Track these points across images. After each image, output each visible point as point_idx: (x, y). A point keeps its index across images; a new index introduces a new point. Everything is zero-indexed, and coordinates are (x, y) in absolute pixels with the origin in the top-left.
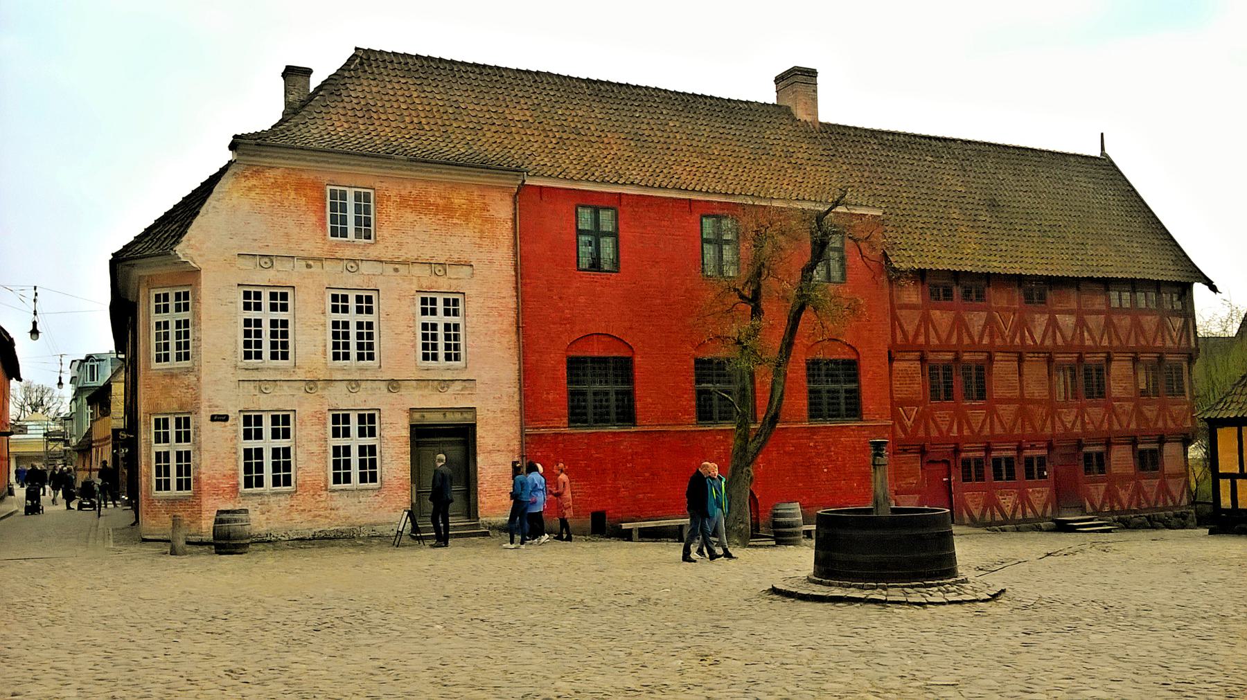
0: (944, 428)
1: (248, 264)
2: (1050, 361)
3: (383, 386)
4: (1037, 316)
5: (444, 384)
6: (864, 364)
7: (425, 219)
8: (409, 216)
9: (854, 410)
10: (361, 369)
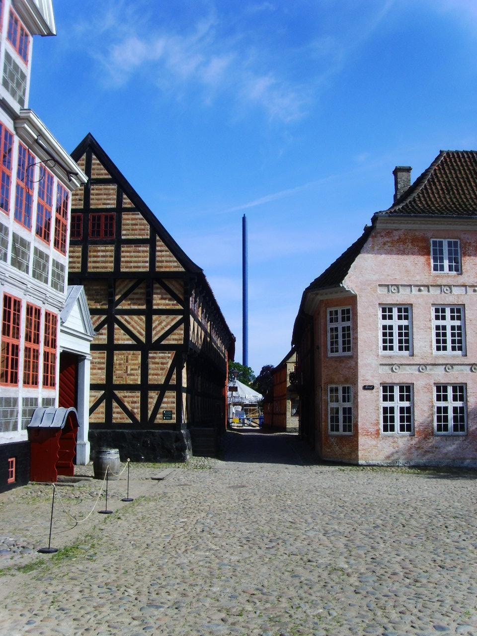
10: (454, 357)
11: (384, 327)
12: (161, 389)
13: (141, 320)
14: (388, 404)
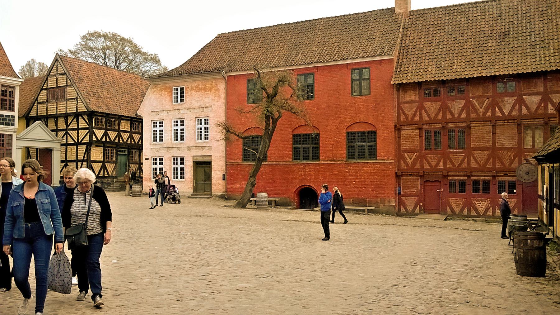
0: (434, 164)
1: (153, 114)
2: (519, 125)
3: (186, 148)
4: (506, 99)
5: (203, 148)
6: (379, 133)
7: (198, 93)
8: (194, 93)
9: (373, 154)
10: (181, 144)
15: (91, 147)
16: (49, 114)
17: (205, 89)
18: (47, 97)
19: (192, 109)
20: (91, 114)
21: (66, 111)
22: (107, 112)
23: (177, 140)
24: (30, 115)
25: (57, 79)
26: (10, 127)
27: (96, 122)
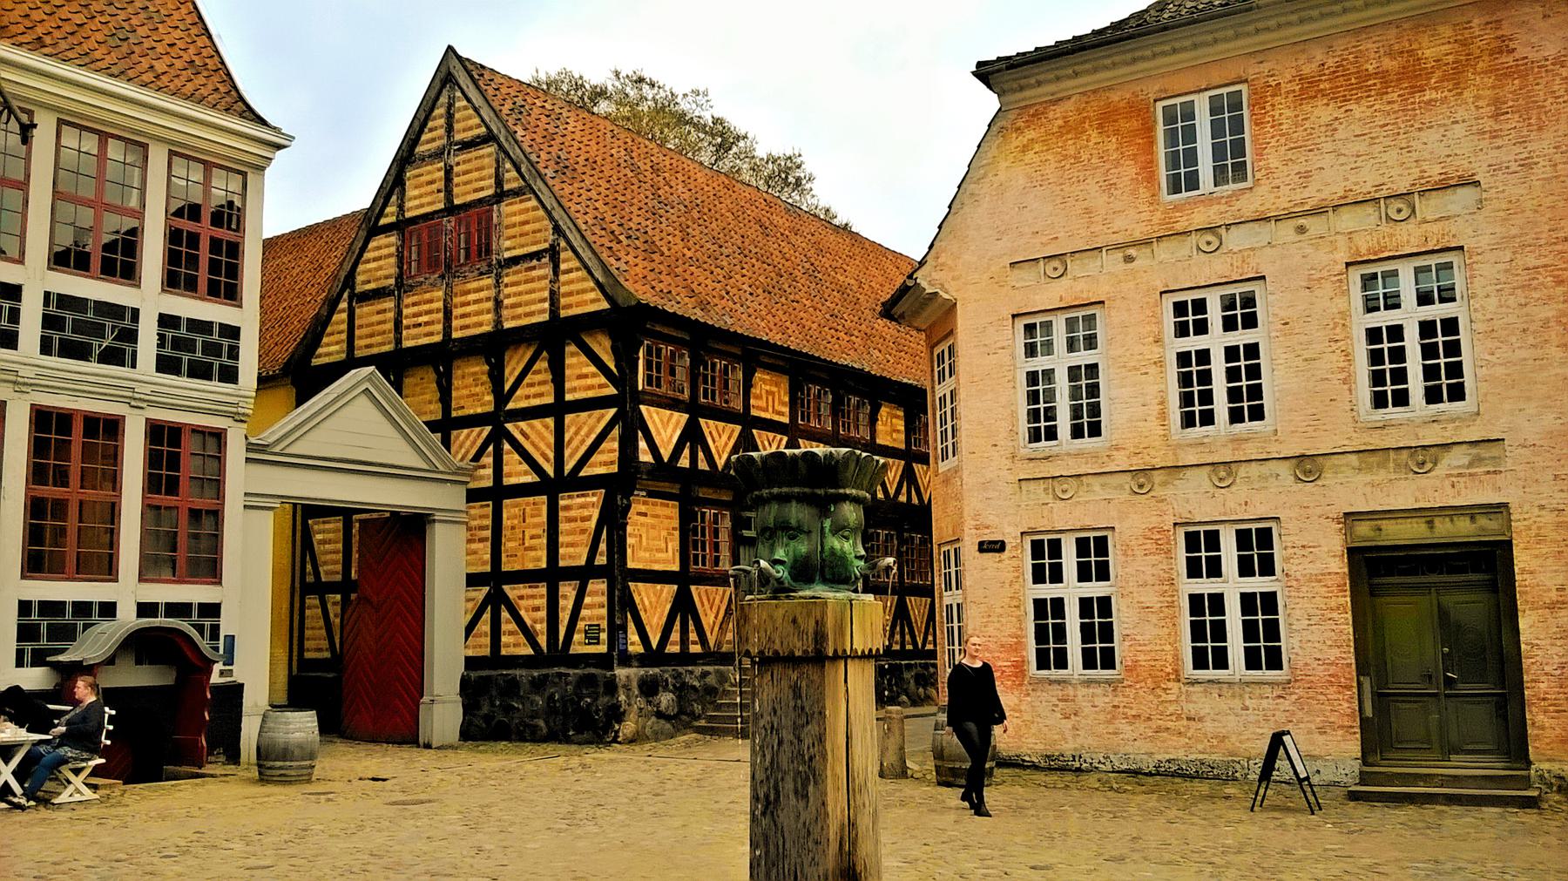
1: (1027, 276)
3: (1284, 469)
5: (1423, 456)
7: (1358, 110)
8: (1322, 112)
10: (1238, 441)
11: (1373, 335)
12: (583, 575)
13: (546, 427)
14: (1048, 591)
15: (628, 494)
16: (407, 344)
17: (1413, 76)
18: (400, 265)
19: (1318, 211)
20: (628, 323)
21: (498, 322)
22: (698, 315)
23: (1208, 418)
24: (315, 362)
25: (448, 172)
26: (215, 386)
27: (649, 366)
